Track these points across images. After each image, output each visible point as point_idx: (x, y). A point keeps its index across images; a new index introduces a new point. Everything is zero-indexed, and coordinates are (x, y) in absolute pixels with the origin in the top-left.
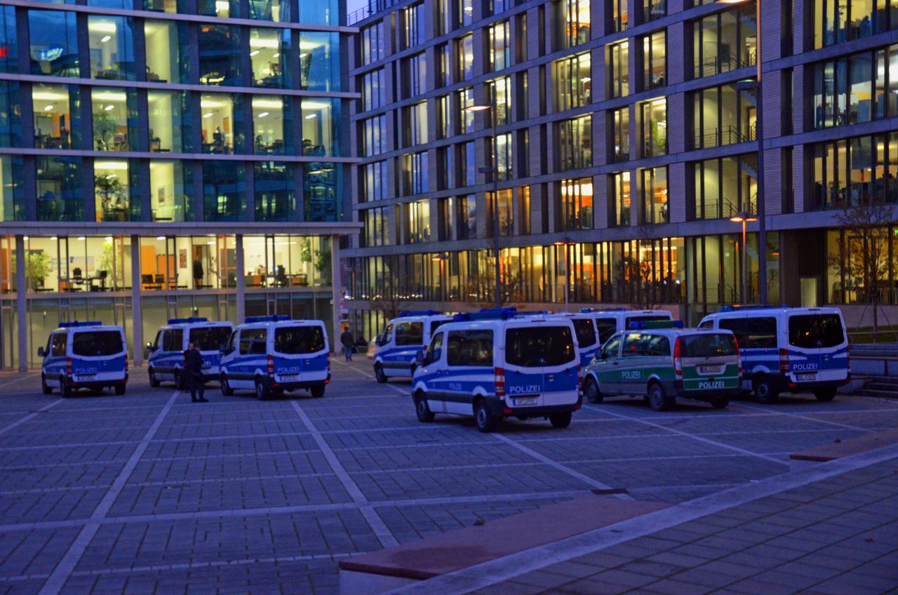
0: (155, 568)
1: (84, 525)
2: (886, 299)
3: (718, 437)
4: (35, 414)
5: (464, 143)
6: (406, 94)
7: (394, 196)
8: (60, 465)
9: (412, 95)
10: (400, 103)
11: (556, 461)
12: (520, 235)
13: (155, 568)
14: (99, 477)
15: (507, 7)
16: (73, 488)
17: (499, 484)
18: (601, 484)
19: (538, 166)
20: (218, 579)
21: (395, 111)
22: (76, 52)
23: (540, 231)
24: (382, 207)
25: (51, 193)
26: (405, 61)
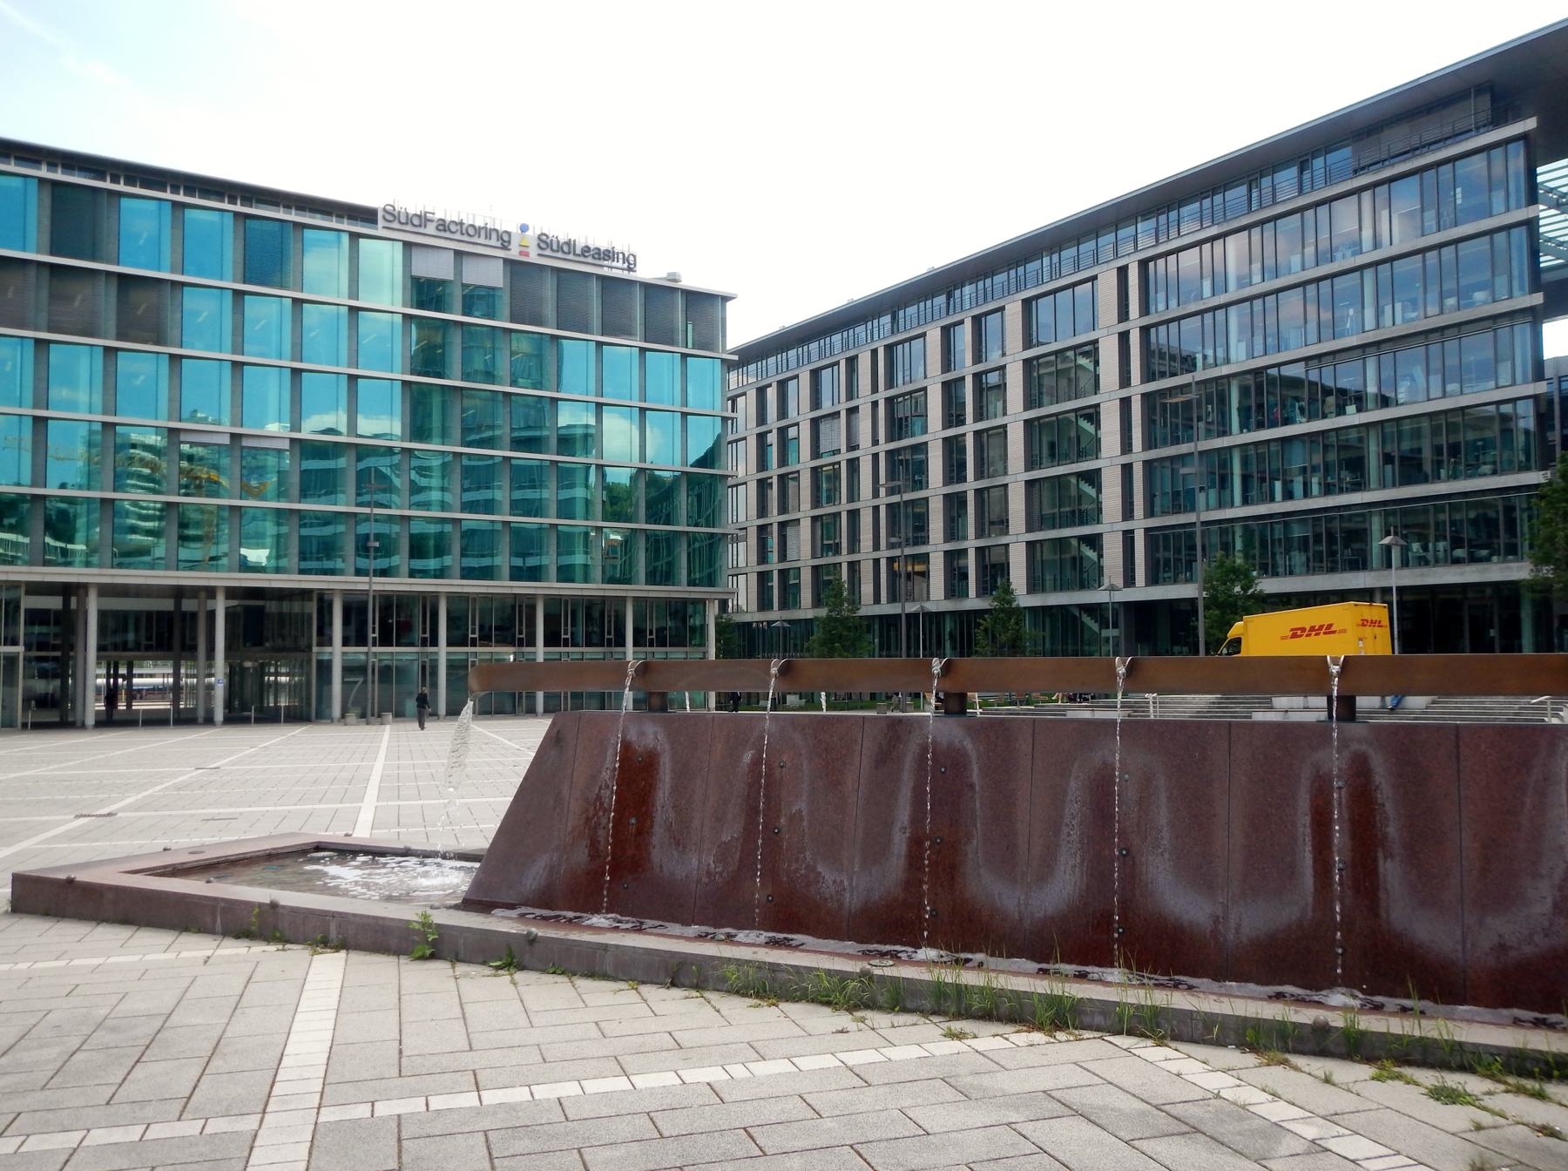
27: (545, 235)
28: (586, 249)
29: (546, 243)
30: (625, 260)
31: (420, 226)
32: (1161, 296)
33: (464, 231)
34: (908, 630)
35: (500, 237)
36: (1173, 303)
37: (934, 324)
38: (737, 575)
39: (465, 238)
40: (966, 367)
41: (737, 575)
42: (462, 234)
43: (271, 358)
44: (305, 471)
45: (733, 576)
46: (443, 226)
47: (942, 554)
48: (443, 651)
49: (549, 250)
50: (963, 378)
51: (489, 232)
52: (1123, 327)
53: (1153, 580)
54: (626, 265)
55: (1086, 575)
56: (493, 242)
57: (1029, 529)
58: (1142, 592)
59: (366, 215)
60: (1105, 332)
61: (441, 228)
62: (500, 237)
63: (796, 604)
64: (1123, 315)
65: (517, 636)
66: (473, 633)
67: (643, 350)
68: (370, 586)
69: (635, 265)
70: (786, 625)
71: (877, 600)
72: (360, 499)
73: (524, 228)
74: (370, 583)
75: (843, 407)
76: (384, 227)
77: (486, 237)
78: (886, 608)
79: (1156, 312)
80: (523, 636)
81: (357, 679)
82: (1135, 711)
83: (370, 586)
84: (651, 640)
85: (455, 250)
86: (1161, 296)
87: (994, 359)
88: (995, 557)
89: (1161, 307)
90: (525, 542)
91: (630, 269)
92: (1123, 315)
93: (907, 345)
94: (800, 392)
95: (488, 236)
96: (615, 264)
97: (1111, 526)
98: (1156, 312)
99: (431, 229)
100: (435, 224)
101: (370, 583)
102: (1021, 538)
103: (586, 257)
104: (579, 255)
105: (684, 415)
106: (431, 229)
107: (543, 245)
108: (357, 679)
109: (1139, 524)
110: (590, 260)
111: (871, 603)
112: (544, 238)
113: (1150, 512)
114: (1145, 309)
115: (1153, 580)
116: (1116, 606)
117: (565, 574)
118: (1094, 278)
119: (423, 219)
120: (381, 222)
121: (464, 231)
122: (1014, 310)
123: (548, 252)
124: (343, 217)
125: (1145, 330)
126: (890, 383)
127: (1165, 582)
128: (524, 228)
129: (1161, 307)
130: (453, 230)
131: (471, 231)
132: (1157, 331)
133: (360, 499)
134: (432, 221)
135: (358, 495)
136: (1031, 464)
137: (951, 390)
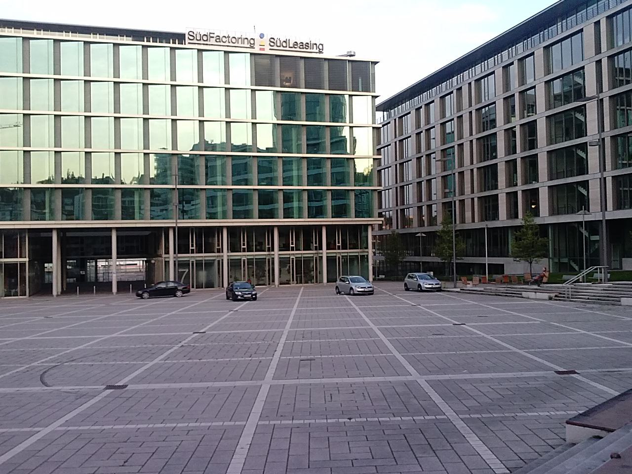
0: (306, 421)
1: (261, 385)
2: (238, 208)
3: (605, 334)
4: (232, 312)
5: (431, 180)
6: (402, 157)
7: (395, 206)
8: (245, 343)
9: (405, 157)
10: (399, 161)
11: (520, 349)
12: (460, 223)
13: (306, 421)
14: (266, 351)
15: (452, 113)
16: (253, 359)
17: (494, 365)
18: (578, 378)
19: (470, 189)
20: (324, 386)
21: (396, 165)
22: (222, 423)
23: (471, 221)
24: (389, 211)
25: (82, 178)
26: (401, 141)
27: (273, 39)
29: (273, 43)
30: (318, 47)
31: (207, 40)
32: (620, 36)
33: (230, 41)
35: (249, 42)
36: (627, 40)
37: (498, 66)
38: (409, 208)
39: (231, 44)
40: (515, 87)
41: (409, 208)
42: (229, 42)
44: (234, 165)
45: (407, 208)
46: (218, 39)
47: (505, 194)
49: (275, 46)
50: (514, 95)
51: (244, 40)
52: (598, 58)
53: (619, 206)
54: (317, 51)
55: (583, 203)
57: (551, 179)
58: (613, 214)
59: (180, 37)
60: (588, 61)
61: (218, 40)
63: (495, 217)
64: (598, 50)
66: (244, 245)
67: (253, 91)
68: (176, 225)
69: (323, 49)
70: (424, 235)
71: (473, 221)
73: (262, 36)
74: (177, 223)
75: (455, 117)
76: (189, 43)
78: (478, 225)
79: (617, 46)
81: (184, 270)
82: (560, 294)
83: (176, 225)
84: (316, 247)
86: (620, 36)
87: (530, 82)
89: (620, 43)
90: (266, 198)
91: (320, 52)
92: (598, 50)
93: (486, 79)
94: (434, 109)
96: (311, 51)
97: (593, 175)
98: (617, 46)
99: (213, 41)
100: (215, 39)
101: (177, 223)
102: (541, 185)
103: (295, 48)
104: (292, 47)
105: (254, 124)
107: (272, 44)
108: (184, 270)
109: (610, 174)
110: (298, 49)
111: (472, 221)
112: (272, 40)
113: (615, 167)
114: (611, 44)
115: (619, 206)
117: (288, 214)
118: (582, 30)
119: (209, 36)
120: (187, 41)
121: (230, 41)
122: (539, 53)
123: (275, 48)
124: (40, 30)
125: (611, 58)
126: (479, 100)
128: (262, 36)
129: (620, 43)
130: (224, 41)
131: (234, 40)
132: (618, 57)
134: (213, 37)
136: (550, 142)
137: (508, 99)
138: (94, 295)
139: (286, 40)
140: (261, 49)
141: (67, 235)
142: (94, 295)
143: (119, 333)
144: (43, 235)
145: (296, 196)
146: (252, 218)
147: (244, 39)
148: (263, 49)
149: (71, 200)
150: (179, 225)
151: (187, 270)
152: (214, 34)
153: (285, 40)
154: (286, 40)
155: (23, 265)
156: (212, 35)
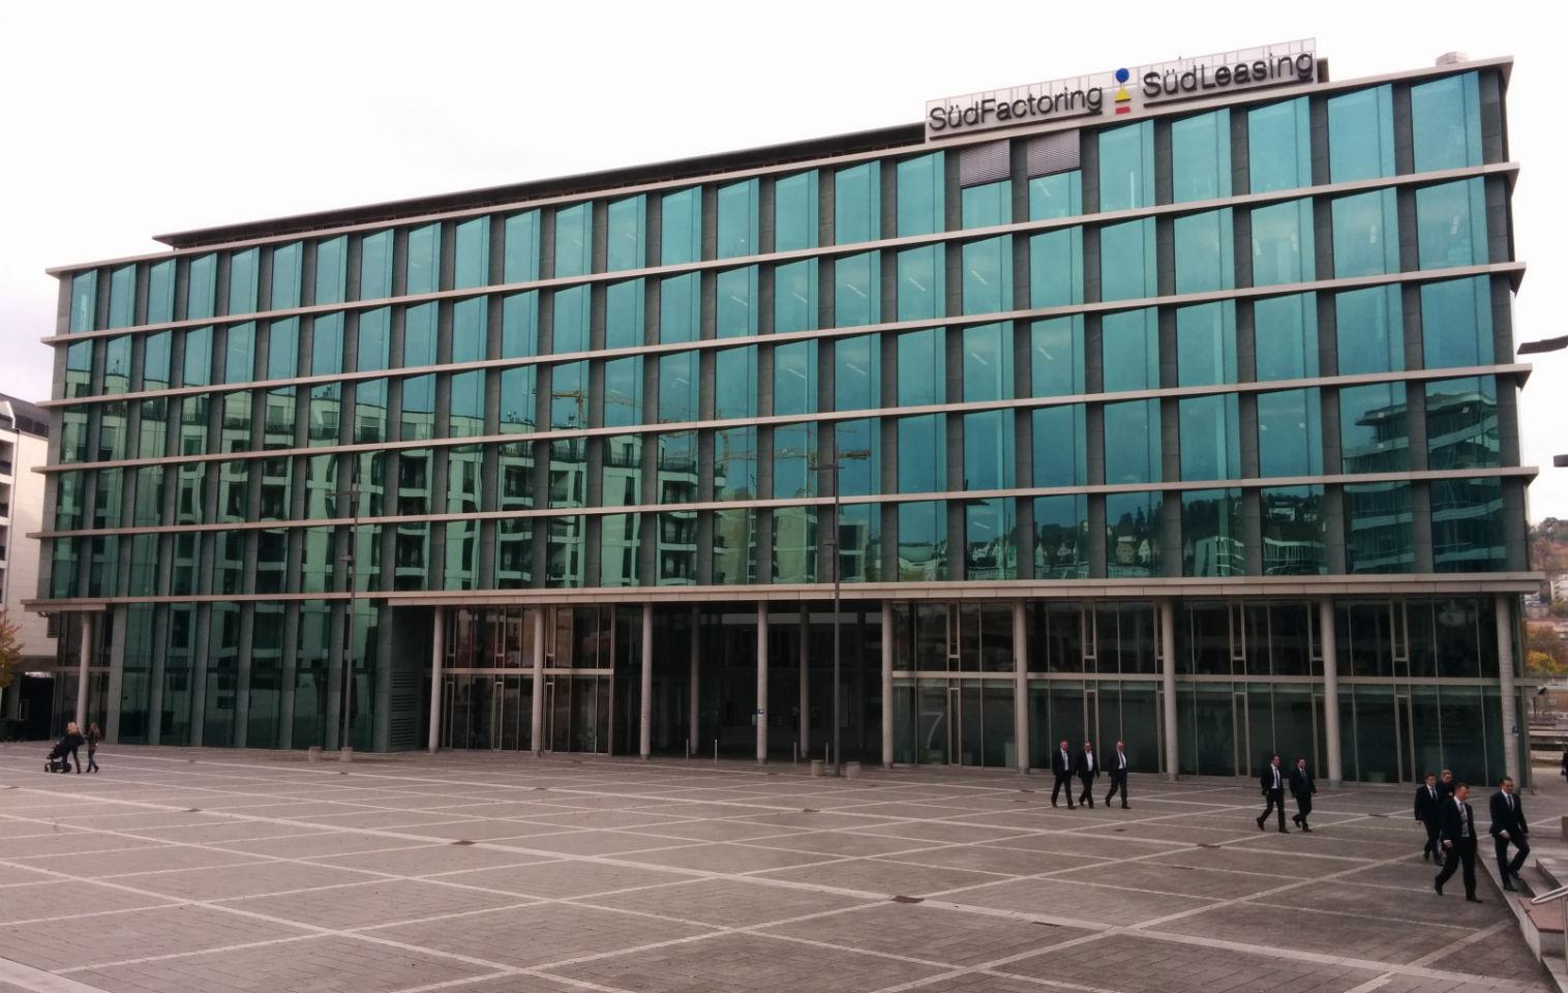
24: (500, 422)
28: (1223, 76)
33: (1035, 109)
34: (1089, 708)
42: (1033, 114)
43: (653, 344)
46: (1005, 113)
48: (536, 673)
56: (1079, 109)
62: (1086, 100)
65: (1395, 659)
68: (837, 595)
72: (1440, 558)
77: (1067, 108)
80: (1406, 659)
83: (837, 595)
85: (1489, 273)
88: (280, 467)
95: (1069, 104)
99: (991, 121)
106: (991, 121)
110: (1232, 87)
116: (938, 754)
127: (375, 591)
133: (1440, 558)
134: (992, 110)
135: (1437, 551)
138: (715, 762)
139: (1195, 70)
140: (1119, 111)
141: (856, 614)
142: (715, 762)
143: (538, 903)
144: (729, 619)
145: (316, 419)
146: (1168, 575)
147: (1073, 95)
148: (1127, 110)
149: (1128, 561)
150: (843, 596)
151: (941, 714)
152: (993, 100)
153: (1191, 69)
154: (1195, 70)
155: (603, 681)
156: (988, 106)
